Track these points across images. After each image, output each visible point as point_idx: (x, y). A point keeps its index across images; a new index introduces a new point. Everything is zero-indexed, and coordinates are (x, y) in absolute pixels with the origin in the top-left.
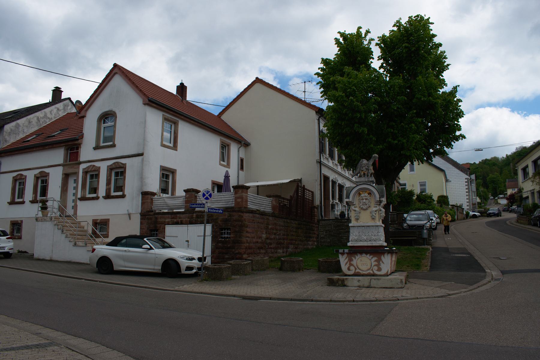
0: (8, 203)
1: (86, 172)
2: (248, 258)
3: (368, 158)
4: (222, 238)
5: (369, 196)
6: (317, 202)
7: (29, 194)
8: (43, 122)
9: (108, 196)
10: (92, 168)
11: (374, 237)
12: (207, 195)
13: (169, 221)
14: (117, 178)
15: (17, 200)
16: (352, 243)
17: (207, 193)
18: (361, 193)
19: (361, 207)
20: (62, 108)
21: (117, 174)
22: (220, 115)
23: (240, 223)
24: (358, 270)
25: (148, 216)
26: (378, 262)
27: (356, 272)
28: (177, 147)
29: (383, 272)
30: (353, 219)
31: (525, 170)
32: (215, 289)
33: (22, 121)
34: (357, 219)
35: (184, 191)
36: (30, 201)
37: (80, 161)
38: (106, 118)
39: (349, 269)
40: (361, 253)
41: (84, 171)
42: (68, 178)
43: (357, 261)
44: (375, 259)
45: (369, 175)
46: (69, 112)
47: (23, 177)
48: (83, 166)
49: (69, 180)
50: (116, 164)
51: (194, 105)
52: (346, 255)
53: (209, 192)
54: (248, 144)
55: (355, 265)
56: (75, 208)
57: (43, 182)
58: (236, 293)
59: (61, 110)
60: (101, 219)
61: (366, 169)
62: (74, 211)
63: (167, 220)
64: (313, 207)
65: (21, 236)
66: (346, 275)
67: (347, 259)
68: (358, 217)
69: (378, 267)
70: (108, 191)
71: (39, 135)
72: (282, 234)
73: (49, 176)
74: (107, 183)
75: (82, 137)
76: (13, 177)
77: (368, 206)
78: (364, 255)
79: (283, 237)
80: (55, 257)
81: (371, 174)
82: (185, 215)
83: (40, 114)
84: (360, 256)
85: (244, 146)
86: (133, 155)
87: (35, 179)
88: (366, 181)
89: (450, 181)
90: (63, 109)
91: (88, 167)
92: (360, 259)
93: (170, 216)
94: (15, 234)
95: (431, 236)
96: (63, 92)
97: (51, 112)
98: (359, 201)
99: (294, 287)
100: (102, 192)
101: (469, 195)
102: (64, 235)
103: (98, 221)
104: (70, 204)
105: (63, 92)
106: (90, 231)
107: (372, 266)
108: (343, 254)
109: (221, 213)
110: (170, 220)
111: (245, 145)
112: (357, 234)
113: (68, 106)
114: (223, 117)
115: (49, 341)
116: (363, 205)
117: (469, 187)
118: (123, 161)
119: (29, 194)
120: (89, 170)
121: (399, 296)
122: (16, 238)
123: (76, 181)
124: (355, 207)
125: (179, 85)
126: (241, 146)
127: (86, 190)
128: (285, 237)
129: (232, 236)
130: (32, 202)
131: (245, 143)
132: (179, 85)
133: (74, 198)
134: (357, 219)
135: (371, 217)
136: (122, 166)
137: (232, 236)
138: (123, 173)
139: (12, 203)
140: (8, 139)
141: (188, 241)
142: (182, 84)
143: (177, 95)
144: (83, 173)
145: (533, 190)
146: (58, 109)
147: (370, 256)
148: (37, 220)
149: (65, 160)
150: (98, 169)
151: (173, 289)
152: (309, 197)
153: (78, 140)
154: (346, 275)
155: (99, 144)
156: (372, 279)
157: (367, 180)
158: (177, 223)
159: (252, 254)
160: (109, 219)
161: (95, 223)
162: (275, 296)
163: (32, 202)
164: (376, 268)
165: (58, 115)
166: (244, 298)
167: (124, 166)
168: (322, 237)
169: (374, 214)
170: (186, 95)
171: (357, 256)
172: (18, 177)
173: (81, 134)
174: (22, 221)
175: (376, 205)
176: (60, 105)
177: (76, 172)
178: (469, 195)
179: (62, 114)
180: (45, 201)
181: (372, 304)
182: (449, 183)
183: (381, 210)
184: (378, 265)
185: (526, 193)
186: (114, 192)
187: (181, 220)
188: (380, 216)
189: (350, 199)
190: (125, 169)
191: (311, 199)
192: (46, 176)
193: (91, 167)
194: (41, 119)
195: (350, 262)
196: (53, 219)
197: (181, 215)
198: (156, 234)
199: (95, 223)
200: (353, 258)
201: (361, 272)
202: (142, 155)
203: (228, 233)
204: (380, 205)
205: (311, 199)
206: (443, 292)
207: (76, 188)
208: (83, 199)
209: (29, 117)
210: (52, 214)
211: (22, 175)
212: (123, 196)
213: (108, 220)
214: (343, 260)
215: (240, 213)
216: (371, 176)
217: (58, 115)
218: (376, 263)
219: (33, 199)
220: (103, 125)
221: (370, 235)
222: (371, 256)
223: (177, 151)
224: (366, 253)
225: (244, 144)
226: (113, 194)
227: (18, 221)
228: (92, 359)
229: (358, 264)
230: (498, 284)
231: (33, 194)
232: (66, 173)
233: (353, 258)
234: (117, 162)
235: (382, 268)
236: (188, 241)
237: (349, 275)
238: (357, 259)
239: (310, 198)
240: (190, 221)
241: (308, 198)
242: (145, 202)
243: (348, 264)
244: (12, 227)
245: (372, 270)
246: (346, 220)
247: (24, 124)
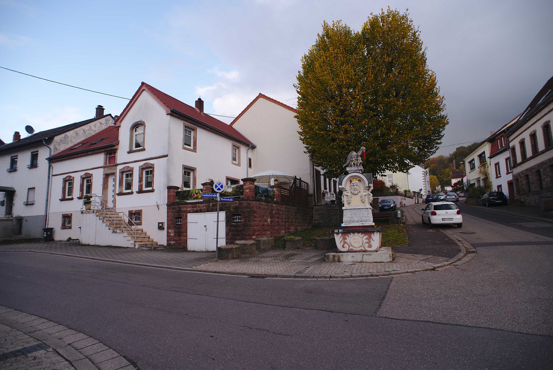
0: (60, 200)
1: (122, 172)
2: (257, 239)
3: (357, 150)
4: (234, 222)
5: (359, 182)
6: (311, 191)
7: (76, 192)
8: (88, 134)
9: (140, 191)
10: (127, 169)
11: (364, 218)
12: (219, 187)
13: (191, 210)
14: (147, 176)
15: (67, 197)
16: (345, 224)
17: (219, 185)
18: (352, 180)
19: (353, 192)
20: (104, 123)
21: (147, 173)
22: (231, 125)
23: (249, 210)
24: (351, 247)
25: (173, 206)
26: (368, 240)
27: (350, 249)
28: (196, 149)
29: (374, 248)
30: (345, 203)
31: (471, 162)
32: (227, 267)
33: (70, 133)
34: (349, 203)
35: (202, 184)
36: (78, 198)
37: (117, 163)
38: (137, 128)
39: (343, 247)
40: (354, 232)
41: (120, 172)
42: (108, 177)
43: (350, 240)
44: (366, 237)
45: (359, 164)
46: (111, 126)
47: (71, 178)
48: (119, 168)
49: (109, 179)
50: (146, 164)
51: (210, 116)
52: (340, 235)
53: (221, 183)
54: (255, 147)
55: (349, 243)
56: (114, 201)
57: (88, 181)
58: (246, 271)
59: (104, 124)
60: (136, 210)
61: (355, 159)
62: (114, 204)
63: (188, 209)
64: (308, 195)
65: (71, 226)
66: (341, 252)
67: (342, 238)
68: (350, 201)
69: (368, 244)
70: (140, 186)
71: (83, 144)
72: (284, 218)
73: (92, 176)
74: (139, 181)
75: (118, 143)
76: (64, 179)
77: (358, 191)
78: (356, 234)
79: (285, 220)
80: (98, 243)
81: (360, 164)
82: (203, 204)
83: (85, 127)
84: (353, 235)
85: (251, 148)
86: (159, 156)
87: (81, 179)
88: (355, 170)
89: (411, 174)
90: (105, 124)
91: (124, 168)
92: (353, 237)
93: (191, 205)
94: (67, 225)
95: (403, 216)
96: (104, 109)
97: (95, 126)
98: (350, 188)
99: (297, 264)
100: (135, 187)
101: (425, 184)
102: (104, 224)
103: (133, 212)
104: (110, 199)
105: (104, 109)
106: (127, 221)
107: (364, 243)
108: (338, 234)
109: (232, 201)
110: (191, 209)
111: (252, 148)
112: (350, 216)
113: (109, 121)
114: (234, 126)
115: (40, 342)
116: (354, 190)
117: (425, 178)
118: (151, 162)
119: (76, 192)
120: (125, 170)
121: (391, 270)
122: (67, 228)
123: (114, 180)
124: (347, 193)
125: (197, 100)
126: (249, 148)
127: (122, 187)
128: (287, 220)
129: (242, 220)
130: (80, 198)
131: (252, 146)
132: (197, 100)
133: (113, 194)
134: (349, 203)
135: (361, 200)
136: (151, 166)
137: (242, 220)
138: (152, 172)
139: (63, 199)
140: (58, 148)
141: (205, 226)
142: (200, 99)
143: (196, 108)
144: (120, 173)
145: (479, 178)
146: (101, 123)
147: (361, 234)
148: (82, 213)
149: (106, 163)
150: (131, 170)
151: (191, 269)
152: (305, 187)
153: (114, 146)
154: (341, 252)
155: (132, 148)
156: (364, 255)
157: (356, 169)
158: (197, 212)
159: (260, 235)
160: (142, 210)
161: (131, 214)
162: (280, 273)
163: (80, 198)
164: (367, 245)
165: (101, 128)
166: (252, 276)
167: (152, 167)
168: (316, 219)
169: (364, 198)
170: (203, 108)
171: (350, 234)
172: (68, 179)
173: (118, 141)
174: (71, 214)
175: (365, 191)
176: (103, 120)
177: (114, 173)
178: (425, 184)
179: (104, 127)
180: (89, 197)
181: (369, 279)
182: (409, 175)
183: (369, 195)
184: (369, 243)
185: (473, 181)
186: (145, 187)
187: (200, 209)
188: (369, 200)
189: (343, 185)
190: (153, 168)
191: (306, 189)
192: (90, 177)
193: (126, 168)
194: (87, 131)
195: (344, 241)
196: (95, 212)
197: (200, 205)
198: (180, 221)
199: (131, 214)
200: (347, 237)
201: (354, 248)
202: (167, 156)
203: (239, 218)
204: (368, 190)
205: (306, 189)
206: (429, 265)
207: (114, 186)
208: (121, 194)
209: (76, 130)
210: (82, 208)
211: (70, 176)
212: (152, 191)
213: (141, 210)
214: (338, 239)
215: (248, 201)
216: (360, 166)
217: (101, 128)
218: (367, 241)
219: (80, 196)
220: (135, 133)
221: (361, 216)
222: (363, 235)
223: (196, 152)
224: (358, 232)
225: (251, 146)
226: (144, 189)
227: (68, 214)
228: (76, 369)
229: (351, 242)
230: (474, 256)
231: (80, 192)
232: (106, 173)
233: (347, 237)
234: (147, 163)
235: (372, 245)
236: (205, 226)
237: (343, 252)
238: (350, 238)
239: (305, 188)
240: (207, 209)
241: (304, 188)
242: (472, 245)
243: (343, 242)
244: (63, 220)
245: (364, 247)
246: (335, 205)
247: (72, 135)
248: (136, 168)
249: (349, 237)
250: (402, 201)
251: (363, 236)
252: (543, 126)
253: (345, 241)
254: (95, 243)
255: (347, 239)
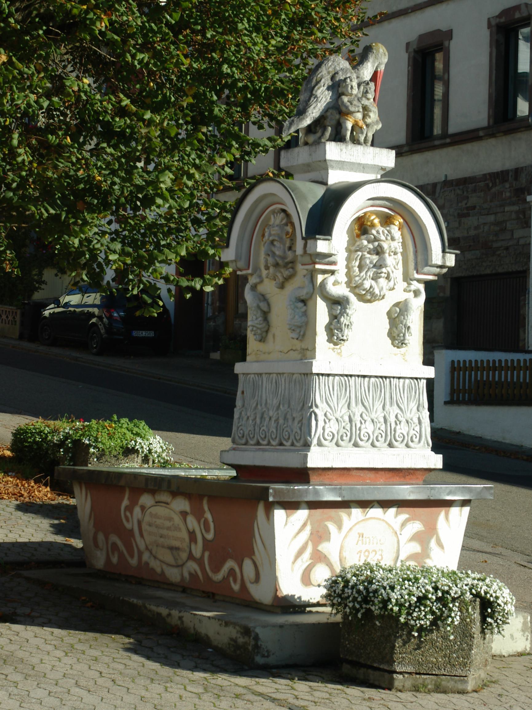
44: (416, 526)
171: (349, 515)
229: (344, 554)
243: (309, 549)
248: (203, 155)
249: (340, 527)
250: (299, 349)
251: (403, 525)
252: (415, 46)
253: (320, 548)
254: (288, 516)
255: (328, 539)
